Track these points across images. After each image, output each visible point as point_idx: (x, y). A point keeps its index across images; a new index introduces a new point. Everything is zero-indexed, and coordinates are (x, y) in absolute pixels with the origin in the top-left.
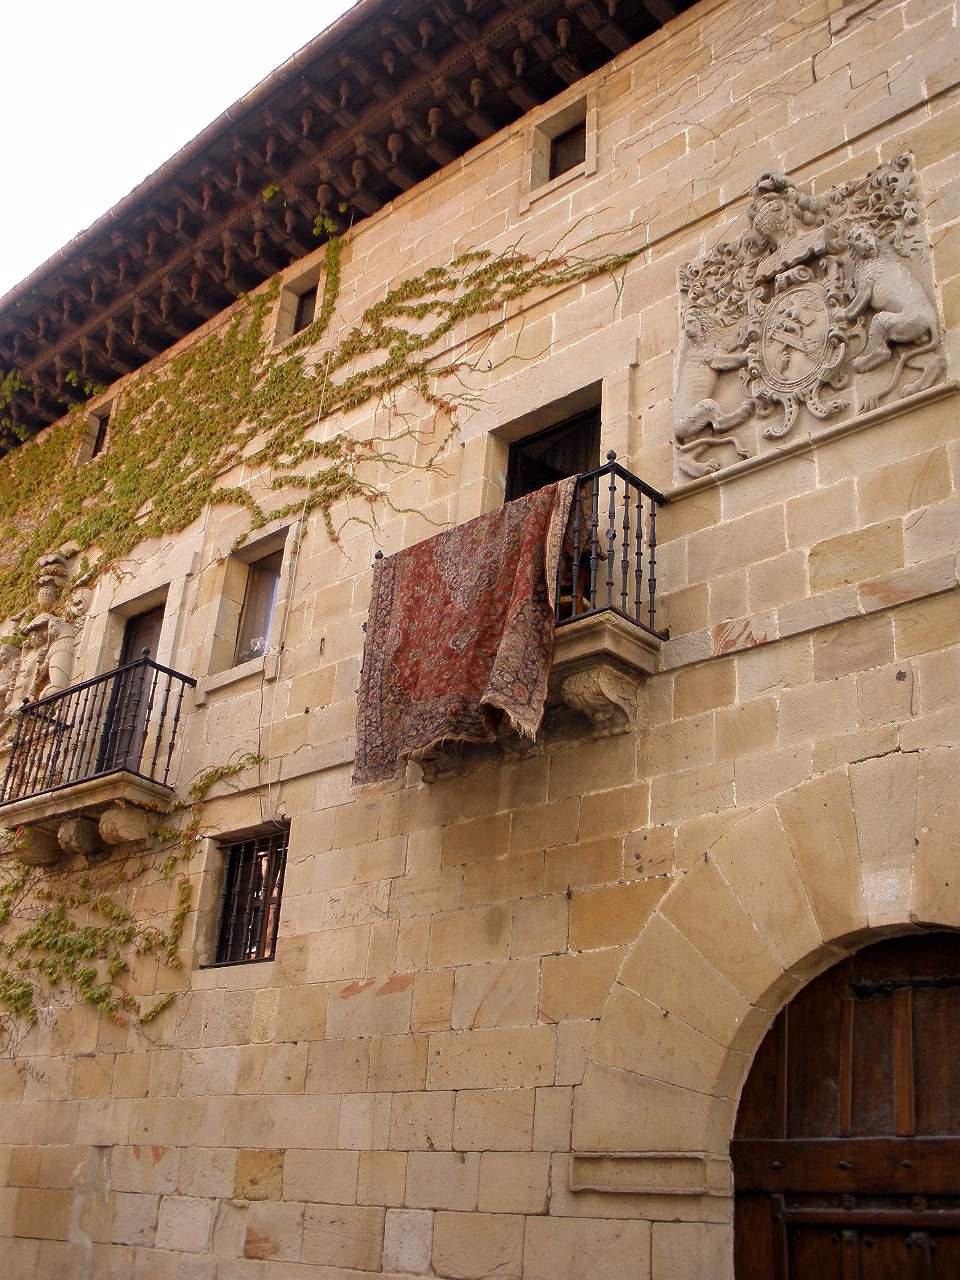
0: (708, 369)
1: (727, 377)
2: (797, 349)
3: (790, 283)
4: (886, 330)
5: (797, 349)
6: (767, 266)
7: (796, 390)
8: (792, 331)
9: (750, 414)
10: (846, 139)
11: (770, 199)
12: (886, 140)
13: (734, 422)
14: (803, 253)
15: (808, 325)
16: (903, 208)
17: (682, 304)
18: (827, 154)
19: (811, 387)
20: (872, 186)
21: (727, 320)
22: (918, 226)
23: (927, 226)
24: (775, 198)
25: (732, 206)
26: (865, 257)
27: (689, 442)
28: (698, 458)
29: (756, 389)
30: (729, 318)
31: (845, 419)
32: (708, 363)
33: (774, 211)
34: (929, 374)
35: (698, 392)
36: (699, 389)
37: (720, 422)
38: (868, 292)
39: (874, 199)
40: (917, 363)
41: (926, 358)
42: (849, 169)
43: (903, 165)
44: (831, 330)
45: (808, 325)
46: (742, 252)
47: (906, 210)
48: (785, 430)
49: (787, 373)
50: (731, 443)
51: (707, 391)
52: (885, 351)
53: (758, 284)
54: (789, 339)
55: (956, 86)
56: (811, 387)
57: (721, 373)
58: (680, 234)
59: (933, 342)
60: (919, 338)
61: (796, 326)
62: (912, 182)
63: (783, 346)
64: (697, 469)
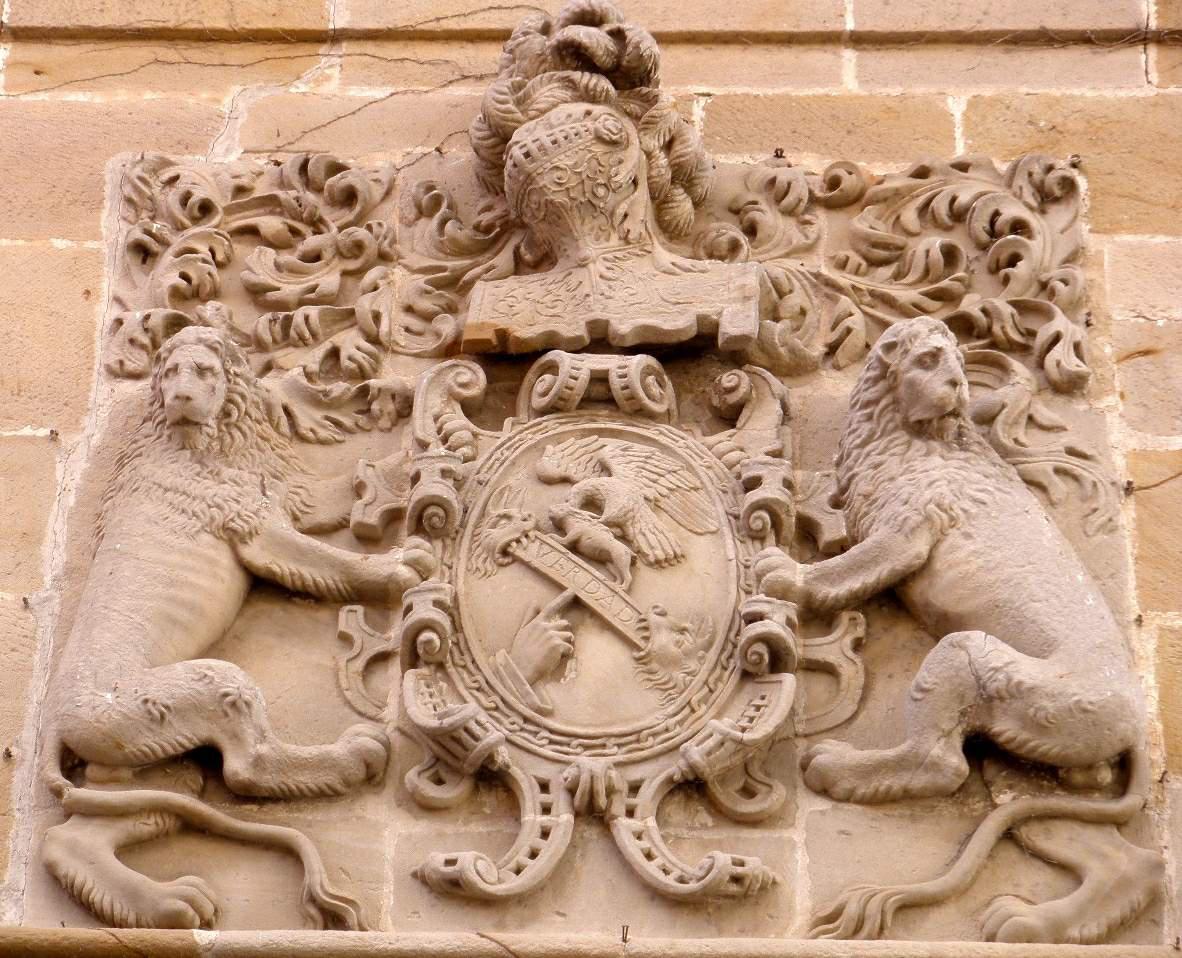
0: (224, 558)
1: (275, 612)
2: (607, 626)
3: (599, 396)
4: (987, 696)
5: (607, 626)
6: (504, 303)
7: (590, 765)
8: (600, 559)
9: (371, 775)
10: (850, 25)
11: (590, 96)
12: (988, 92)
13: (306, 780)
14: (678, 322)
15: (658, 564)
16: (1045, 332)
17: (115, 297)
18: (1084, 39)
19: (635, 773)
20: (924, 210)
21: (309, 418)
22: (1081, 406)
23: (1113, 420)
24: (607, 101)
25: (370, 47)
26: (920, 429)
27: (101, 783)
28: (127, 850)
29: (416, 700)
30: (319, 415)
31: (756, 930)
32: (233, 537)
33: (599, 139)
34: (1102, 897)
35: (174, 622)
36: (183, 615)
37: (258, 762)
38: (920, 546)
39: (937, 255)
40: (1060, 842)
41: (1094, 837)
42: (842, 119)
43: (1054, 193)
44: (753, 618)
45: (658, 564)
46: (390, 217)
47: (1056, 339)
48: (512, 884)
49: (552, 693)
50: (287, 852)
51: (204, 634)
52: (957, 761)
53: (452, 350)
54: (582, 580)
55: (22, 35)
56: (635, 773)
57: (262, 586)
58: (142, 52)
59: (1131, 801)
60: (1090, 767)
61: (619, 550)
62: (1071, 259)
63: (559, 600)
64: (133, 895)
